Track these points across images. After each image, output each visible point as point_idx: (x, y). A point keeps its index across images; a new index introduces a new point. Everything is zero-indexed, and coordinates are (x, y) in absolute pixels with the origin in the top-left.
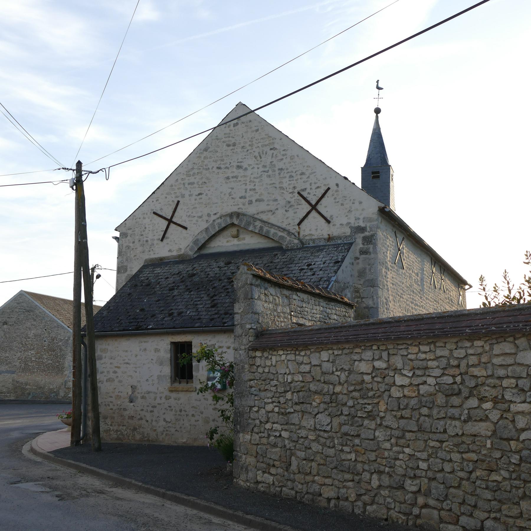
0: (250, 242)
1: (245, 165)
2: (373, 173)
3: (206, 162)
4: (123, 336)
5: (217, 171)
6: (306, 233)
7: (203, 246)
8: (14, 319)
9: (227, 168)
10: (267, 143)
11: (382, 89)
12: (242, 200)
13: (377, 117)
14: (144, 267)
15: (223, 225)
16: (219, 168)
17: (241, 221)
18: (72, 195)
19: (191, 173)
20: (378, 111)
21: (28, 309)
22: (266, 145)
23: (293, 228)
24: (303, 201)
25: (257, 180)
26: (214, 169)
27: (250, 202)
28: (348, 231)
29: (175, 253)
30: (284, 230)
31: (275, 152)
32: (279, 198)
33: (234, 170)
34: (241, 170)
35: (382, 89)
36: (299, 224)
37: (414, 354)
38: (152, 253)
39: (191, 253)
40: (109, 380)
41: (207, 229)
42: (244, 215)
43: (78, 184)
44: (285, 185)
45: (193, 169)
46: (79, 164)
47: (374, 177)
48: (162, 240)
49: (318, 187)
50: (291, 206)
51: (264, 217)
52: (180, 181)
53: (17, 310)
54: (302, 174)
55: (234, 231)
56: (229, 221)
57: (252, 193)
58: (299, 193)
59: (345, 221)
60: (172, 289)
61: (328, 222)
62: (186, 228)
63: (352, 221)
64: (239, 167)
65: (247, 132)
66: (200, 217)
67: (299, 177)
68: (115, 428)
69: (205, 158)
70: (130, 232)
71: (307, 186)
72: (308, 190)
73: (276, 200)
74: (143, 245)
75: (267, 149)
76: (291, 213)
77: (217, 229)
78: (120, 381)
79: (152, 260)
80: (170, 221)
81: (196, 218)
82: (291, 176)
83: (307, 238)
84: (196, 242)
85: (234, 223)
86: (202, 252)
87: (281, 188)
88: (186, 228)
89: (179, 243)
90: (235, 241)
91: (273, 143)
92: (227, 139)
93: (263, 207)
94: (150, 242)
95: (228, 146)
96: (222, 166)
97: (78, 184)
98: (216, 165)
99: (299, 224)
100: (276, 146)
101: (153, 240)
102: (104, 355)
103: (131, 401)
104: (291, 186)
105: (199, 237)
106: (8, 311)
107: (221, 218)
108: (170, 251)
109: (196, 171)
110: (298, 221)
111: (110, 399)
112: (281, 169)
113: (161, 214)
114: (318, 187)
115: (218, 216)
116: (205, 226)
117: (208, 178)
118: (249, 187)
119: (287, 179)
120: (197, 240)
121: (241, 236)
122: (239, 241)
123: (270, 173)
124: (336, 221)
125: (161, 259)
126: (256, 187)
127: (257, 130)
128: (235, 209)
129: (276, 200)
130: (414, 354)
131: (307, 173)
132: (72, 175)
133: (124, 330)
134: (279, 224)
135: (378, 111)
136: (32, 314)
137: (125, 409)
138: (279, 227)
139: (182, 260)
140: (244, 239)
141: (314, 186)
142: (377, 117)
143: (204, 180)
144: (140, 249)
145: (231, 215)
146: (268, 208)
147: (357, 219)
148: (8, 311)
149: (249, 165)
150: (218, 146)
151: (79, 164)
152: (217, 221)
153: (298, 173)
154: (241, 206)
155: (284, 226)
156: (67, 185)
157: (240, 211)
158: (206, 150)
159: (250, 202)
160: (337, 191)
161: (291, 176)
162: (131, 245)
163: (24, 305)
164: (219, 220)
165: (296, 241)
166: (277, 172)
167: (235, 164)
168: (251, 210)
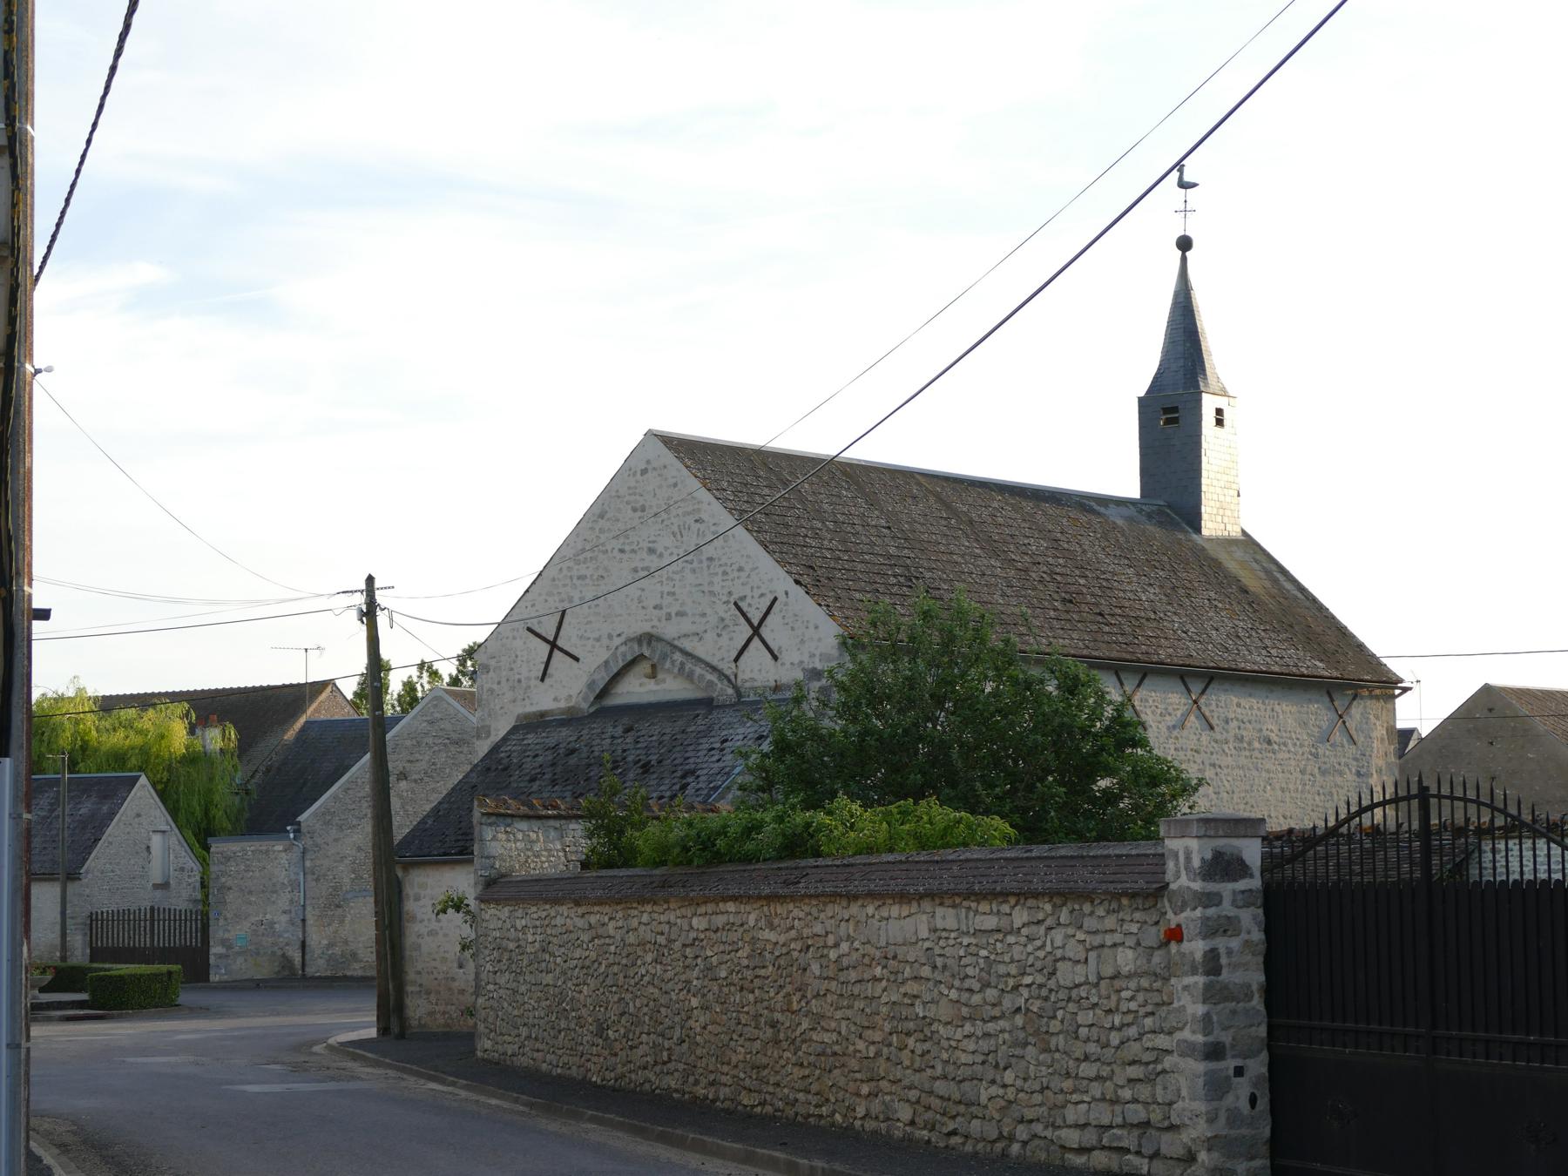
0: (670, 688)
1: (660, 549)
2: (1166, 411)
3: (603, 538)
4: (445, 863)
5: (619, 556)
6: (747, 676)
7: (604, 692)
8: (423, 765)
9: (633, 551)
10: (690, 508)
11: (1195, 185)
12: (656, 612)
13: (1184, 260)
14: (514, 730)
15: (629, 658)
16: (622, 551)
17: (654, 651)
18: (362, 631)
19: (581, 558)
20: (1185, 244)
21: (455, 736)
22: (689, 514)
23: (728, 668)
24: (742, 620)
25: (677, 577)
26: (616, 552)
27: (669, 617)
28: (800, 676)
29: (563, 705)
30: (714, 669)
31: (702, 527)
32: (708, 611)
33: (644, 555)
34: (654, 557)
35: (1195, 185)
36: (736, 660)
37: (1549, 849)
38: (527, 702)
39: (585, 706)
40: (432, 933)
41: (606, 663)
42: (659, 639)
43: (369, 614)
44: (716, 588)
45: (583, 551)
46: (370, 580)
47: (1168, 421)
48: (542, 680)
49: (762, 595)
50: (725, 627)
51: (687, 645)
52: (565, 572)
53: (430, 741)
54: (741, 569)
55: (644, 667)
56: (637, 650)
57: (670, 599)
58: (736, 604)
59: (796, 658)
60: (533, 780)
61: (775, 658)
62: (577, 659)
63: (806, 658)
64: (651, 551)
65: (660, 487)
66: (598, 640)
67: (736, 574)
68: (442, 1008)
69: (602, 531)
70: (492, 663)
71: (747, 591)
72: (748, 600)
73: (704, 615)
74: (513, 688)
75: (690, 520)
76: (724, 641)
77: (621, 664)
78: (446, 935)
79: (526, 716)
80: (553, 645)
81: (591, 642)
82: (725, 573)
83: (748, 685)
84: (591, 685)
85: (647, 652)
86: (605, 705)
87: (712, 593)
88: (577, 659)
89: (567, 689)
90: (651, 685)
91: (699, 510)
92: (632, 498)
93: (686, 626)
94: (524, 684)
95: (635, 510)
96: (627, 548)
97: (369, 614)
98: (617, 544)
99: (736, 660)
100: (704, 516)
101: (529, 679)
102: (423, 893)
103: (461, 967)
104: (725, 591)
105: (596, 677)
106: (408, 743)
107: (625, 643)
108: (555, 699)
109: (588, 555)
110: (735, 654)
111: (434, 964)
112: (710, 559)
113: (538, 630)
114: (762, 595)
115: (622, 639)
116: (605, 655)
117: (606, 569)
118: (666, 589)
119: (720, 577)
120: (593, 682)
121: (660, 676)
122: (657, 683)
123: (695, 565)
124: (785, 657)
125: (542, 714)
126: (676, 590)
127: (675, 485)
128: (646, 628)
129: (704, 615)
130: (1549, 849)
131: (747, 568)
132: (360, 600)
133: (445, 854)
134: (708, 659)
135: (1185, 244)
136: (465, 749)
137: (453, 979)
138: (708, 664)
139: (571, 719)
140: (664, 681)
141: (757, 593)
142: (1184, 260)
143: (601, 572)
144: (509, 695)
145: (640, 639)
146: (694, 629)
147: (812, 656)
148: (408, 743)
149: (666, 548)
150: (619, 510)
151: (370, 580)
152: (623, 649)
153: (735, 567)
154: (655, 623)
155: (715, 662)
156: (354, 614)
157: (654, 631)
158: (601, 516)
159: (669, 617)
160: (786, 604)
161: (725, 573)
162: (495, 687)
163: (446, 725)
164: (623, 649)
165: (730, 691)
166: (705, 564)
167: (645, 545)
168: (669, 631)
